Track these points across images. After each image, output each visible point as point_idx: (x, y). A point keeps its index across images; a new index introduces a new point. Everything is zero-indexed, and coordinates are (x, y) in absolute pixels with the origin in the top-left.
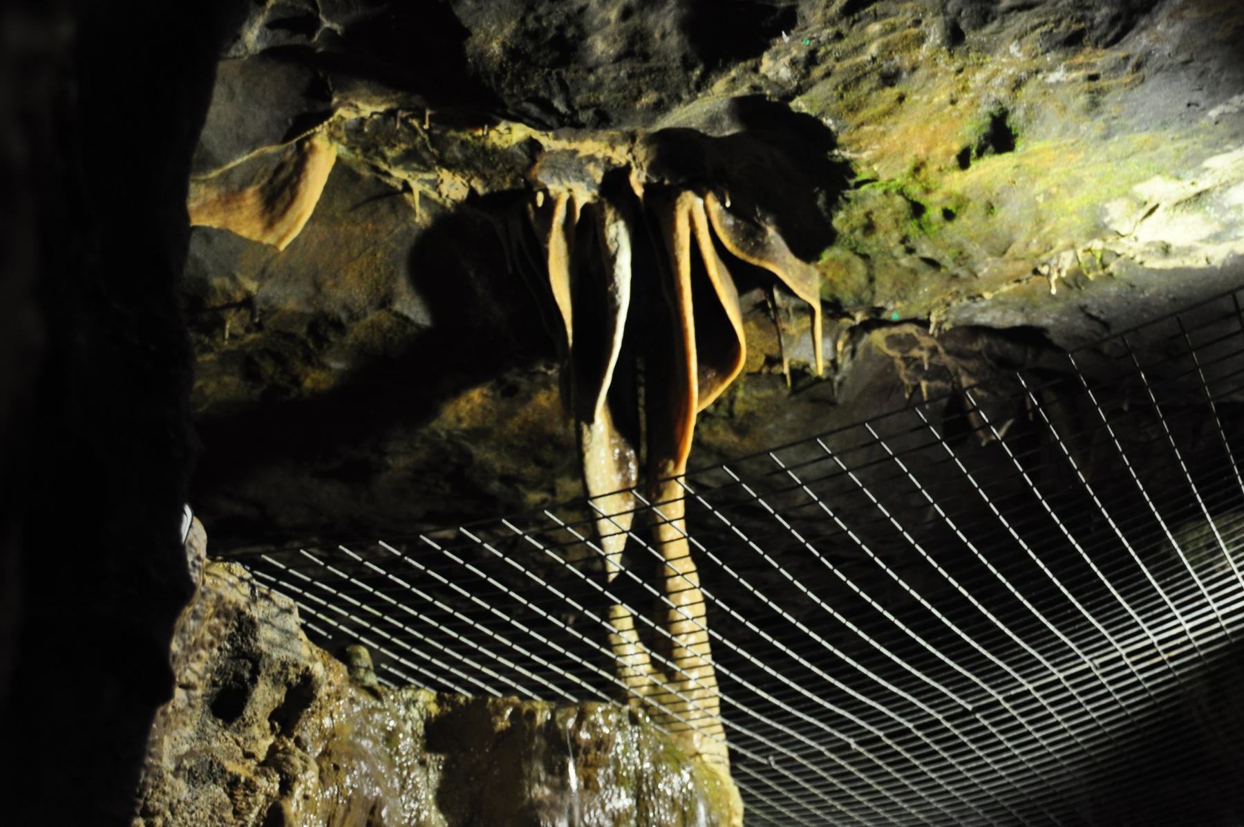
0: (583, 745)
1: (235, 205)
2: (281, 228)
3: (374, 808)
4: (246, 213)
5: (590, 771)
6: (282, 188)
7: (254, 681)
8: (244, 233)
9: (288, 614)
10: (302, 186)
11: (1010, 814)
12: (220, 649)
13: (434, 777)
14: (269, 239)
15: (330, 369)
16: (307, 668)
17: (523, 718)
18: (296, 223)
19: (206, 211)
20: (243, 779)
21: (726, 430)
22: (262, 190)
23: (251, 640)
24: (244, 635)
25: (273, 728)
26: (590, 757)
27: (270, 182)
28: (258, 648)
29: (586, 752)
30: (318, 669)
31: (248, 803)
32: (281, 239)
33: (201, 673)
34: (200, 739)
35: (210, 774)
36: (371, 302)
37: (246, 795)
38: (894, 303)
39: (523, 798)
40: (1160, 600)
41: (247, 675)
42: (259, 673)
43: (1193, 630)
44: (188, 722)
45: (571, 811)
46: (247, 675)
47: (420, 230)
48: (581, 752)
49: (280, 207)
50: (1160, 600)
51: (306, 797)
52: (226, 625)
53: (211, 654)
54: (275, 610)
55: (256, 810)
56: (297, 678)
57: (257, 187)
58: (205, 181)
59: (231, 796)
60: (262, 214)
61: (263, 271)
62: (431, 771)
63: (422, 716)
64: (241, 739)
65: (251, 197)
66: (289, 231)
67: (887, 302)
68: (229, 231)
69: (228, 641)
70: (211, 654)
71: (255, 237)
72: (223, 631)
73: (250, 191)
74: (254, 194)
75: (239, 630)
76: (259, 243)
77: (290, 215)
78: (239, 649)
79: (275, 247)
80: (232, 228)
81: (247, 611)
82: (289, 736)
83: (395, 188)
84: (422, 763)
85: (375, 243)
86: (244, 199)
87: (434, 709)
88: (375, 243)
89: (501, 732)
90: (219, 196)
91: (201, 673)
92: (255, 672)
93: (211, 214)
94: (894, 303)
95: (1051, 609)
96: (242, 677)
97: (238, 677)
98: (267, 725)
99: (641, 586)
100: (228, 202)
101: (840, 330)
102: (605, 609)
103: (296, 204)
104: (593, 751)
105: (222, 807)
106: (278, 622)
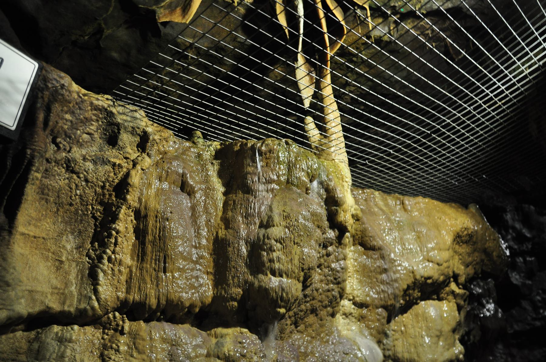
0: (264, 152)
1: (173, 14)
2: (187, 17)
3: (183, 176)
4: (177, 15)
5: (268, 160)
6: (187, 6)
7: (119, 133)
8: (176, 21)
9: (135, 112)
10: (192, 3)
11: (468, 176)
12: (102, 122)
13: (216, 167)
14: (184, 21)
15: (227, 64)
16: (144, 129)
17: (243, 145)
18: (191, 15)
19: (165, 17)
20: (117, 164)
21: (364, 67)
22: (182, 8)
23: (114, 119)
24: (110, 117)
25: (138, 150)
26: (267, 156)
27: (184, 5)
28: (117, 121)
29: (265, 154)
30: (150, 130)
31: (119, 171)
32: (187, 20)
33: (95, 130)
34: (100, 151)
35: (207, 182)
36: (231, 40)
37: (119, 169)
38: (398, 3)
39: (244, 171)
40: (492, 82)
41: (116, 131)
42: (120, 130)
43: (507, 89)
44: (93, 146)
45: (259, 174)
46: (116, 131)
47: (243, 15)
48: (263, 154)
49: (186, 11)
50: (492, 82)
51: (142, 170)
52: (101, 114)
53: (98, 124)
54: (128, 110)
55: (122, 173)
56: (141, 132)
57: (180, 7)
58: (162, 7)
59: (113, 169)
60: (182, 15)
61: (195, 35)
62: (215, 166)
63: (214, 149)
64: (121, 153)
65: (179, 11)
66: (189, 17)
67: (395, 3)
68: (172, 21)
69: (105, 119)
70: (98, 124)
71: (180, 22)
72: (101, 116)
73: (178, 9)
74: (180, 9)
75: (107, 115)
76: (181, 23)
77: (189, 13)
78: (109, 122)
79: (185, 23)
80: (173, 20)
81: (108, 109)
82: (145, 152)
83: (230, 2)
84: (212, 163)
85: (230, 22)
86: (176, 11)
87: (219, 147)
88: (230, 22)
89: (237, 151)
90: (169, 12)
91: (95, 130)
92: (119, 130)
93: (166, 18)
94: (398, 3)
95: (471, 102)
96: (115, 131)
97: (113, 132)
98: (136, 149)
99: (286, 100)
100: (172, 13)
101: (390, 22)
102: (302, 121)
103: (191, 9)
104: (268, 154)
105: (110, 172)
106: (129, 114)
